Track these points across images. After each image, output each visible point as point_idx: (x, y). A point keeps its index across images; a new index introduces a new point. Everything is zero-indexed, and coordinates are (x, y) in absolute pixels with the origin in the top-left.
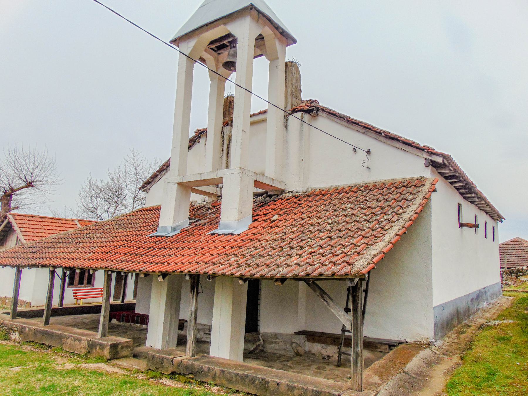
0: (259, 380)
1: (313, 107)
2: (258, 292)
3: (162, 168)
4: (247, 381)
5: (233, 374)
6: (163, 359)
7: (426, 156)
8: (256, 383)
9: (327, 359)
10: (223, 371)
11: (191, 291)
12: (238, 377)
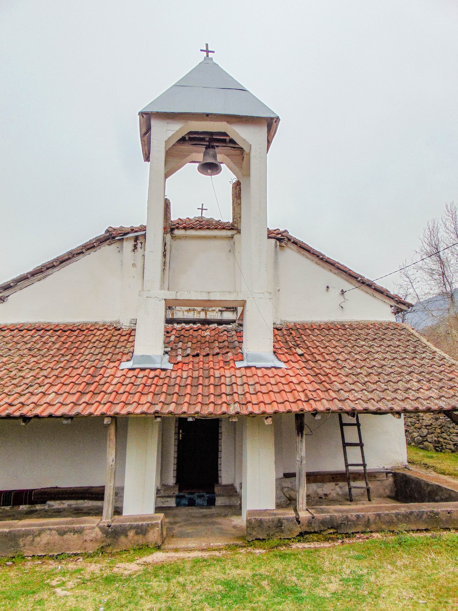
0: (427, 513)
1: (284, 236)
2: (218, 437)
3: (41, 269)
4: (412, 518)
5: (393, 515)
6: (280, 521)
7: (393, 303)
8: (424, 517)
9: (323, 497)
10: (379, 515)
11: (298, 433)
12: (400, 516)
